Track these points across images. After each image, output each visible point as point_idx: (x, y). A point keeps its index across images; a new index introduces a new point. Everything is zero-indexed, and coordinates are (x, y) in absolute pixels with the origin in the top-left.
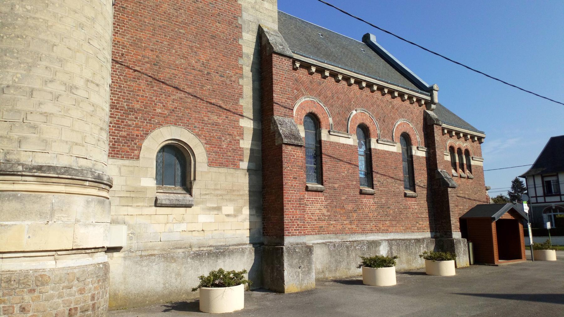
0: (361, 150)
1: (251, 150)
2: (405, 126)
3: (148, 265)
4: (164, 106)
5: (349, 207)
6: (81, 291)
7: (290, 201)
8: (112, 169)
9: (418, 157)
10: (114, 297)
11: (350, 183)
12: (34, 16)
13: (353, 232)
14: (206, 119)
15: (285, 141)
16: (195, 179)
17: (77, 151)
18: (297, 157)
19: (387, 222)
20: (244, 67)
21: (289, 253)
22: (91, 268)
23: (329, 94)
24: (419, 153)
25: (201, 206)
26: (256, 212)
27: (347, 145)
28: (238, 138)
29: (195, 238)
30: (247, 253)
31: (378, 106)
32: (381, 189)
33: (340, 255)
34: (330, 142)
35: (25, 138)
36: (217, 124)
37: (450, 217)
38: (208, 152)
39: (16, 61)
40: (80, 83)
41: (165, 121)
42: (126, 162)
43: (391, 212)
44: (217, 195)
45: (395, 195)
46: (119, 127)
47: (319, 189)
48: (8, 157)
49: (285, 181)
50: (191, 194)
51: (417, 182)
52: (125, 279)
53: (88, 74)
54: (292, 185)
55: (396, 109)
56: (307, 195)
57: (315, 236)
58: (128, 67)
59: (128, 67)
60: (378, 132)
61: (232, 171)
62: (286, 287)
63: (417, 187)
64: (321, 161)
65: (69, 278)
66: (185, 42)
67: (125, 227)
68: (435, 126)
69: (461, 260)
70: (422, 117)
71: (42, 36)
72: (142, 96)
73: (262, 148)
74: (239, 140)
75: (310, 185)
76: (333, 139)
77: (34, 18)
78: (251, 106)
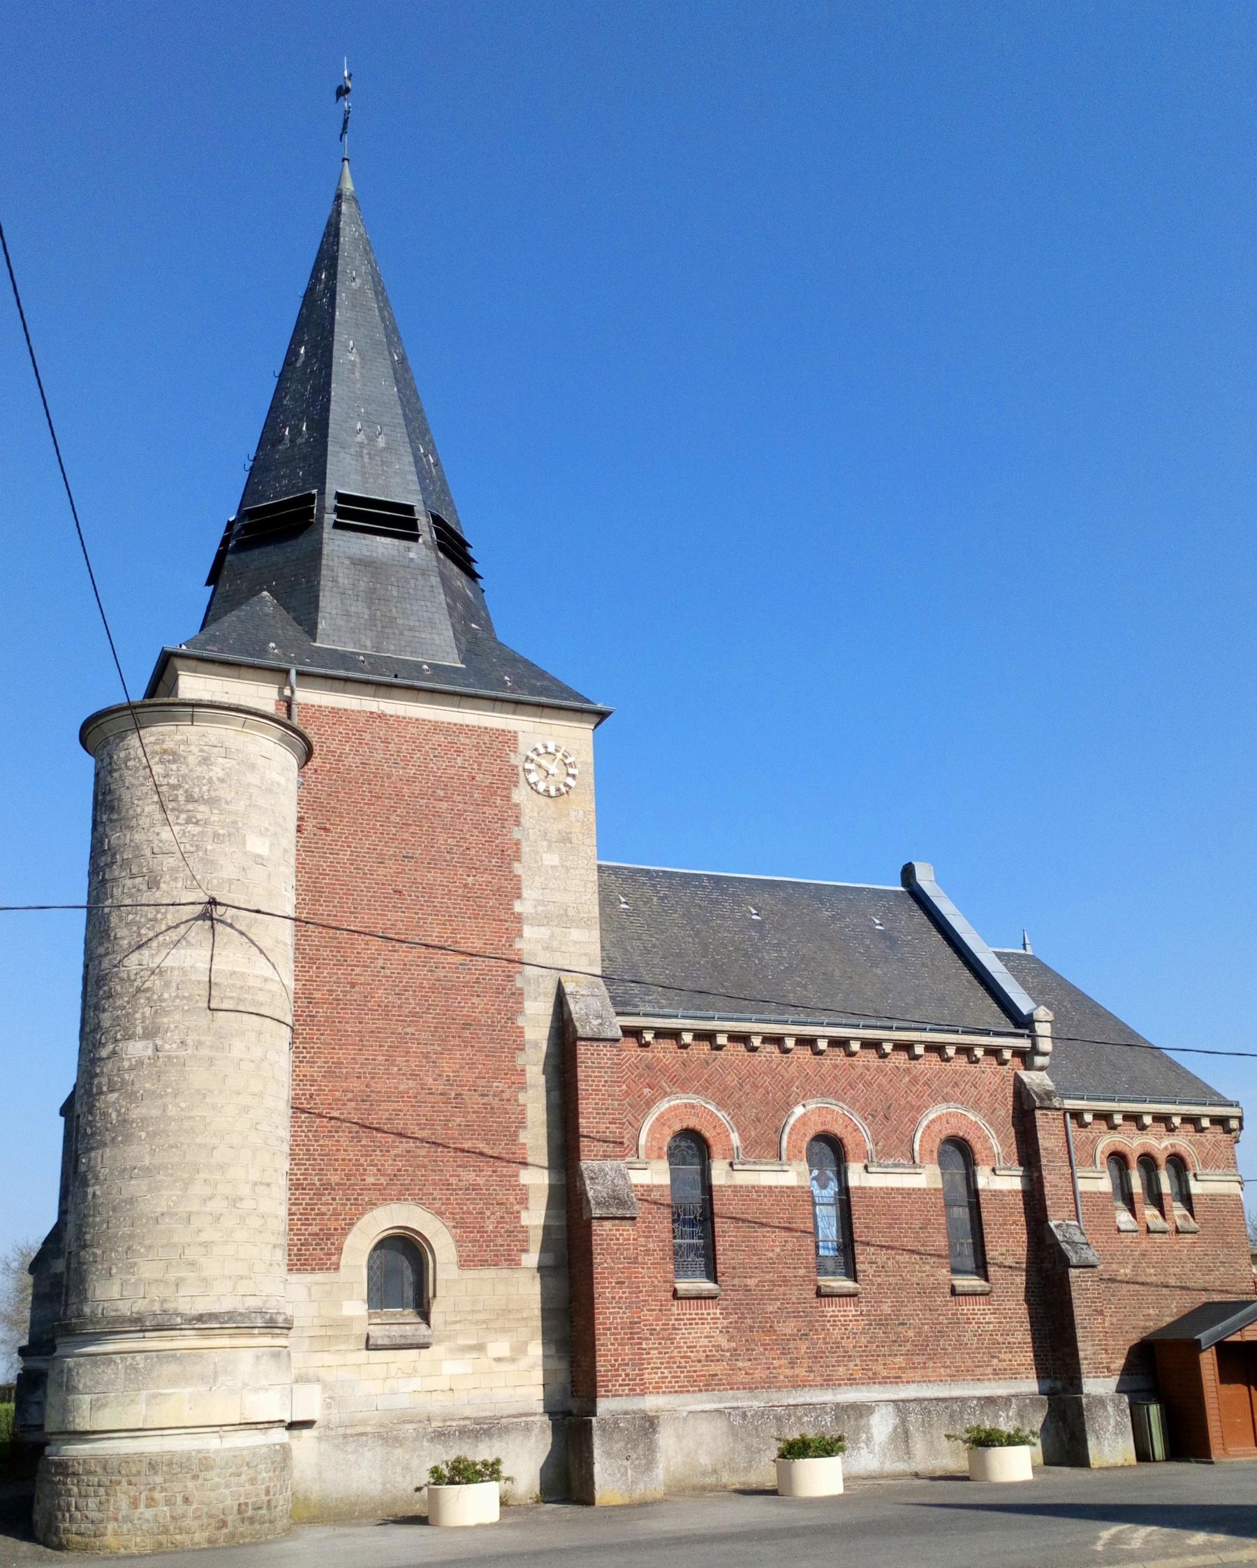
0: (825, 1192)
1: (546, 1228)
2: (952, 1120)
3: (355, 1451)
4: (379, 1170)
5: (789, 1328)
6: (253, 1481)
7: (609, 1329)
8: (295, 1295)
9: (996, 1194)
10: (300, 1501)
11: (789, 1273)
12: (188, 1114)
13: (797, 1384)
14: (453, 1180)
15: (597, 1212)
16: (435, 1296)
17: (244, 1287)
18: (625, 1240)
19: (899, 1359)
20: (528, 1068)
21: (604, 1430)
22: (264, 1450)
23: (731, 1080)
24: (1000, 1181)
25: (447, 1344)
26: (557, 1351)
27: (782, 1187)
28: (517, 1208)
29: (437, 1404)
30: (536, 1430)
31: (869, 1084)
32: (879, 1280)
33: (758, 1436)
34: (735, 1187)
35: (182, 1279)
36: (476, 1187)
37: (1076, 1341)
38: (459, 1242)
39: (170, 1179)
40: (245, 1190)
41: (384, 1195)
42: (320, 1277)
43: (911, 1333)
44: (477, 1323)
45: (924, 1292)
46: (307, 1219)
47: (705, 1294)
48: (166, 1306)
49: (598, 1289)
50: (428, 1324)
51: (992, 1253)
52: (320, 1473)
53: (255, 1175)
54: (613, 1298)
55: (925, 1084)
56: (676, 1308)
57: (699, 1395)
58: (320, 1116)
59: (320, 1116)
60: (870, 1146)
61: (505, 1273)
62: (598, 1495)
63: (991, 1270)
64: (713, 1232)
65: (241, 1463)
66: (414, 1047)
67: (317, 1388)
68: (1038, 1113)
69: (1107, 1449)
70: (1010, 1091)
71: (199, 1140)
72: (343, 1160)
73: (568, 1220)
74: (518, 1212)
75: (683, 1286)
76: (876, 1181)
77: (190, 1118)
78: (543, 1142)
